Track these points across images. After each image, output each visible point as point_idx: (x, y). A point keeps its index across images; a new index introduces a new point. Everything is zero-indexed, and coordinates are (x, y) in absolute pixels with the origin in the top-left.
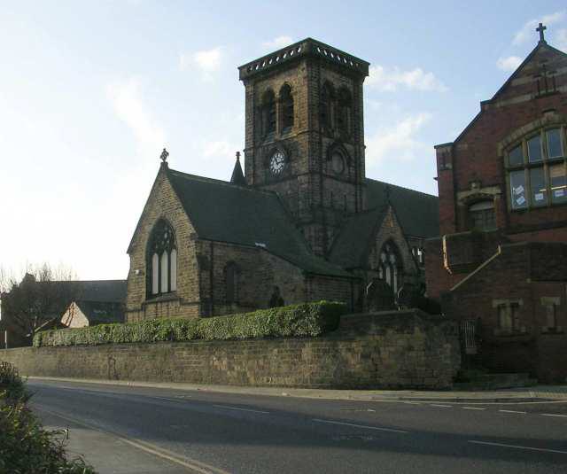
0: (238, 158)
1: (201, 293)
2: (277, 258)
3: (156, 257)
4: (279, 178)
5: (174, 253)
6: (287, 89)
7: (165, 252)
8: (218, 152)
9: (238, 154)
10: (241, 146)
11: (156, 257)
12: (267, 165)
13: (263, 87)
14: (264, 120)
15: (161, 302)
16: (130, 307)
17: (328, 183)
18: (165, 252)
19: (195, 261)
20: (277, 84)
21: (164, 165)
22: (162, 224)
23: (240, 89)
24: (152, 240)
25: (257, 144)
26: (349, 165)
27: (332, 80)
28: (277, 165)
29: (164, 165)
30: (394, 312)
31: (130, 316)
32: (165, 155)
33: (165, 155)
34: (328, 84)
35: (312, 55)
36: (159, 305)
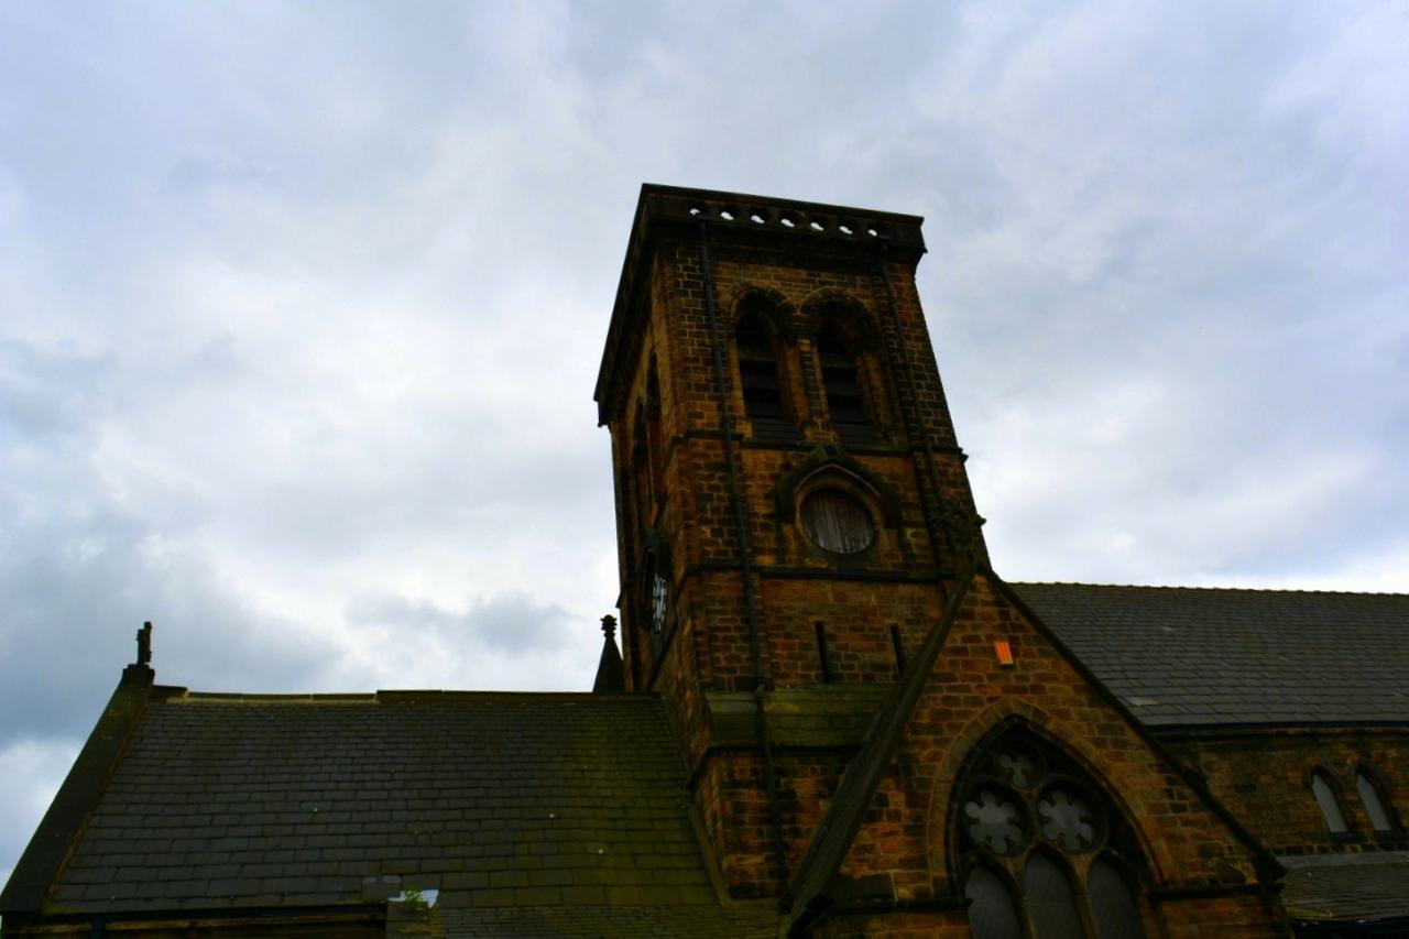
0: (609, 636)
9: (608, 623)
17: (794, 597)
26: (894, 522)
27: (776, 285)
34: (755, 301)
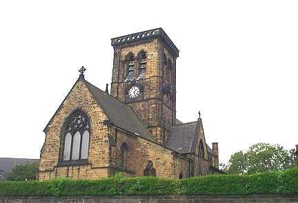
1: (110, 161)
2: (151, 143)
3: (69, 136)
4: (134, 101)
5: (86, 134)
6: (143, 54)
7: (78, 133)
8: (102, 77)
9: (107, 85)
10: (109, 82)
11: (69, 136)
12: (127, 92)
13: (125, 52)
14: (125, 68)
15: (85, 163)
16: (41, 169)
17: (164, 105)
18: (78, 133)
19: (107, 139)
20: (136, 50)
21: (82, 77)
22: (78, 112)
23: (111, 51)
24: (71, 120)
25: (120, 81)
28: (134, 92)
29: (82, 77)
30: (24, 182)
31: (41, 175)
32: (83, 70)
33: (83, 70)
35: (160, 37)
36: (71, 168)
